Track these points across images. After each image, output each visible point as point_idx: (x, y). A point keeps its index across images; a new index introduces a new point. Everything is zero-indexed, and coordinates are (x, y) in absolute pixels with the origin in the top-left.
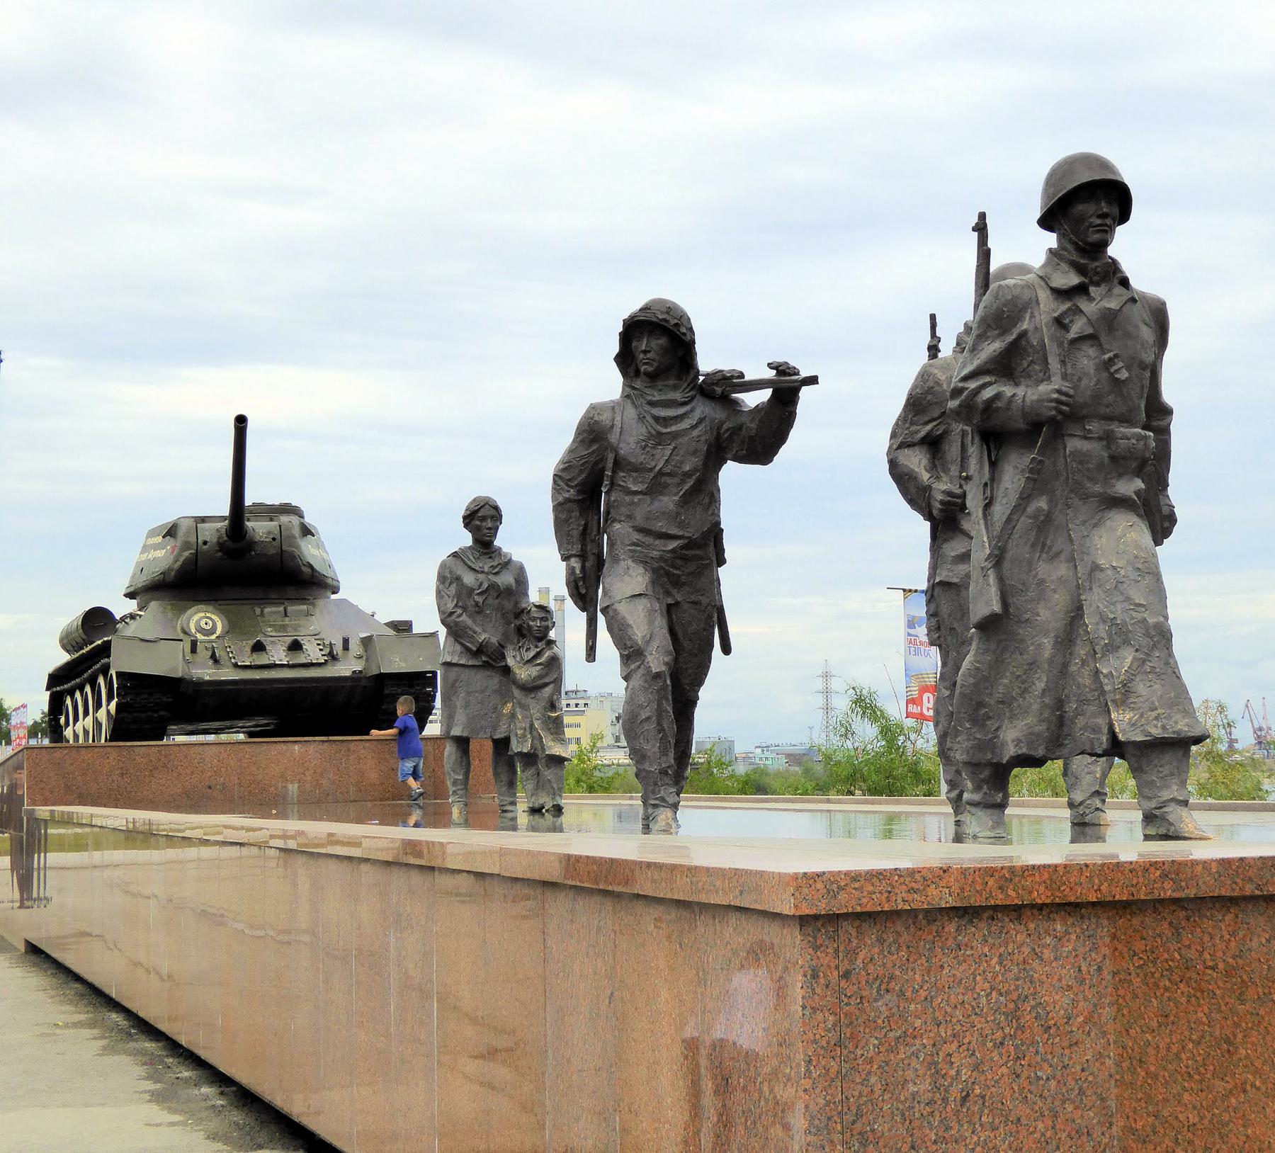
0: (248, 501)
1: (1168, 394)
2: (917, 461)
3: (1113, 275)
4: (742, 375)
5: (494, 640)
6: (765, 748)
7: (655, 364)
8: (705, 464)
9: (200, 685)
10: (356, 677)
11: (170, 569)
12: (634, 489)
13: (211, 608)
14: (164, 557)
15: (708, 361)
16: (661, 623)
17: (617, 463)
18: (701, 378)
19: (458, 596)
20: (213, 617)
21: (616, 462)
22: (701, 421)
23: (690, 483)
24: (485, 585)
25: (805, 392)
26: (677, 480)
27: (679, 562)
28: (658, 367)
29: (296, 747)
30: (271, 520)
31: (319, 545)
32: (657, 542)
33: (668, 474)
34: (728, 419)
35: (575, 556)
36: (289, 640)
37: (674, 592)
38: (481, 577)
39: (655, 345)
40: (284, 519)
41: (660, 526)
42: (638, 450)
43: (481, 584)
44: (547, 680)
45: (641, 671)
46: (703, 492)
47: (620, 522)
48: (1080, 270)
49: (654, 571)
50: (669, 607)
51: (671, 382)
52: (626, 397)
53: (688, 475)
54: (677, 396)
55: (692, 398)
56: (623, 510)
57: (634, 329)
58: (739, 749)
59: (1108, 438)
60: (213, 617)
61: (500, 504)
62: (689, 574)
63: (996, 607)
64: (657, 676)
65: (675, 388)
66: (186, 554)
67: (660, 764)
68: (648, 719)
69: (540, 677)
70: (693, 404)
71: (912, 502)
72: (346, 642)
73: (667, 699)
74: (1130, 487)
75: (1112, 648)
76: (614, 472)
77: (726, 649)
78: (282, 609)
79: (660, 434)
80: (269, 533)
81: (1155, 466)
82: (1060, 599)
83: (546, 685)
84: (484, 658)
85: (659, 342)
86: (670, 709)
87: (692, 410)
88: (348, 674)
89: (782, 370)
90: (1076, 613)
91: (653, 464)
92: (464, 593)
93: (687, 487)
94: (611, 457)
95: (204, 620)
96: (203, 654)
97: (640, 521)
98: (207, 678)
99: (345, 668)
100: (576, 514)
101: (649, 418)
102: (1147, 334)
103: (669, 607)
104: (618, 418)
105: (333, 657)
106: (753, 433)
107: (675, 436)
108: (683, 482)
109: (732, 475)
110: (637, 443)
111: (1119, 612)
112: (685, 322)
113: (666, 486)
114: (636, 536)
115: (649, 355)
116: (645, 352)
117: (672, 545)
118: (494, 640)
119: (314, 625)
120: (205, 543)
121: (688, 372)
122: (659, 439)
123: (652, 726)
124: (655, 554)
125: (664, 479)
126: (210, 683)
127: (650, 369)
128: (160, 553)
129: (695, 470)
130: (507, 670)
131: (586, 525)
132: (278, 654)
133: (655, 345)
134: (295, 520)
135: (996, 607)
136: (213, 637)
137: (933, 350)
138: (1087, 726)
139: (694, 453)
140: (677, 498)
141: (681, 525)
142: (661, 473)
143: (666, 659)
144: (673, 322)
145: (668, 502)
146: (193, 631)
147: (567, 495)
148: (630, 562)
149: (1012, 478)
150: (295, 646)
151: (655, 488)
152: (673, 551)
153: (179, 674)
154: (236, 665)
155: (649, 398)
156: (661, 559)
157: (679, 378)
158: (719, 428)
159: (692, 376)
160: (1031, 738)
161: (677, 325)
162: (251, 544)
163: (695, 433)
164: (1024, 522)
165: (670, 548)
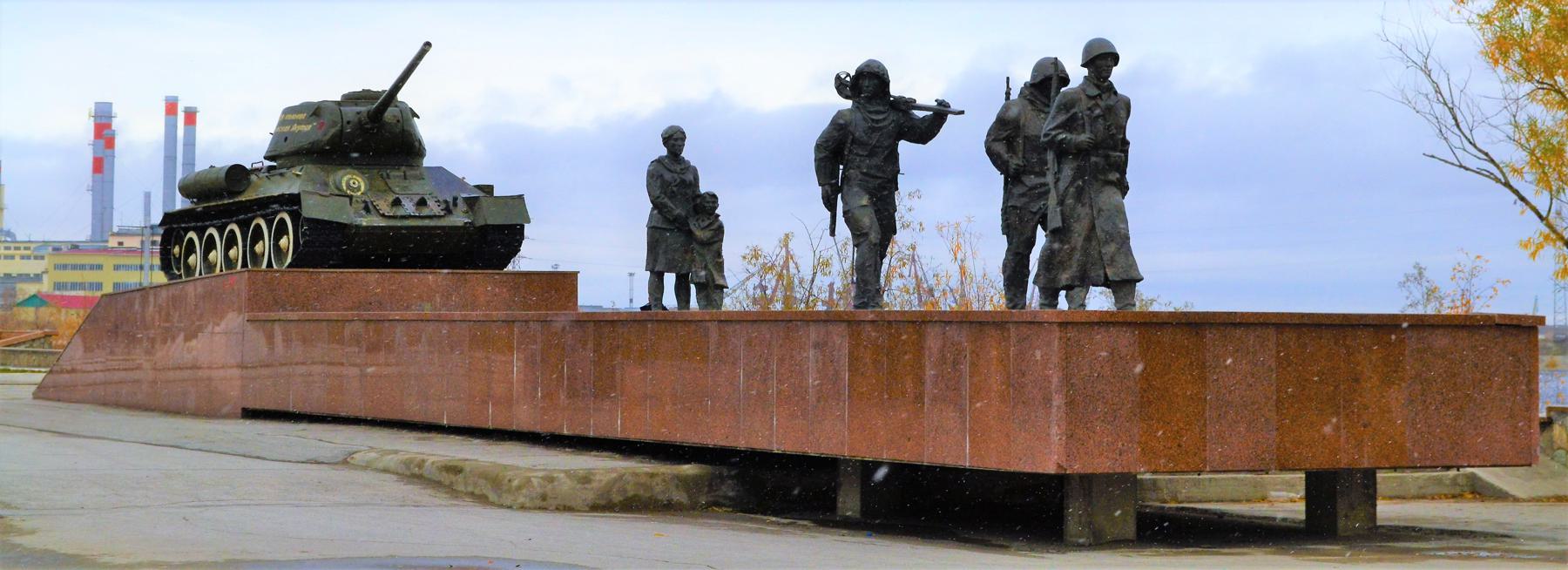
0: (401, 96)
1: (1128, 137)
2: (1000, 148)
3: (1111, 89)
10: (465, 227)
15: (895, 90)
17: (853, 141)
19: (662, 187)
39: (867, 85)
48: (1098, 87)
59: (1107, 157)
63: (1060, 224)
66: (333, 131)
71: (995, 163)
72: (455, 199)
74: (1114, 176)
75: (1107, 242)
81: (1122, 167)
82: (1085, 223)
90: (1093, 228)
95: (353, 180)
99: (459, 219)
102: (1123, 114)
105: (448, 211)
107: (880, 129)
109: (906, 150)
111: (1108, 228)
122: (873, 130)
128: (306, 128)
130: (690, 233)
135: (1060, 224)
137: (1008, 94)
138: (1096, 273)
145: (876, 161)
149: (1068, 171)
150: (422, 203)
160: (1073, 278)
164: (1072, 190)
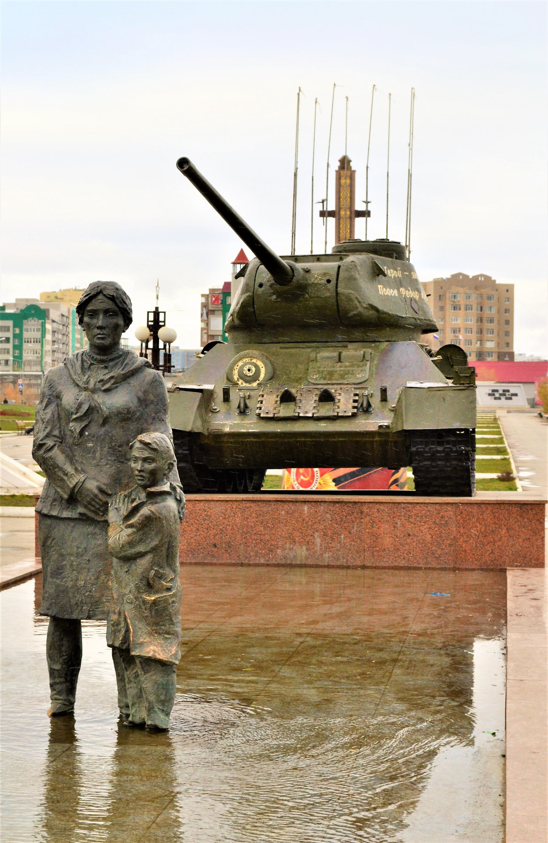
5: (92, 485)
9: (218, 436)
10: (383, 432)
13: (256, 352)
20: (260, 364)
24: (85, 407)
29: (306, 508)
38: (84, 395)
43: (80, 406)
44: (141, 548)
60: (260, 364)
61: (54, 291)
66: (245, 296)
69: (131, 544)
78: (336, 354)
80: (325, 274)
83: (141, 555)
84: (81, 510)
88: (374, 428)
92: (62, 417)
98: (227, 430)
105: (365, 409)
118: (92, 485)
120: (261, 285)
136: (255, 384)
146: (236, 377)
150: (326, 397)
153: (188, 429)
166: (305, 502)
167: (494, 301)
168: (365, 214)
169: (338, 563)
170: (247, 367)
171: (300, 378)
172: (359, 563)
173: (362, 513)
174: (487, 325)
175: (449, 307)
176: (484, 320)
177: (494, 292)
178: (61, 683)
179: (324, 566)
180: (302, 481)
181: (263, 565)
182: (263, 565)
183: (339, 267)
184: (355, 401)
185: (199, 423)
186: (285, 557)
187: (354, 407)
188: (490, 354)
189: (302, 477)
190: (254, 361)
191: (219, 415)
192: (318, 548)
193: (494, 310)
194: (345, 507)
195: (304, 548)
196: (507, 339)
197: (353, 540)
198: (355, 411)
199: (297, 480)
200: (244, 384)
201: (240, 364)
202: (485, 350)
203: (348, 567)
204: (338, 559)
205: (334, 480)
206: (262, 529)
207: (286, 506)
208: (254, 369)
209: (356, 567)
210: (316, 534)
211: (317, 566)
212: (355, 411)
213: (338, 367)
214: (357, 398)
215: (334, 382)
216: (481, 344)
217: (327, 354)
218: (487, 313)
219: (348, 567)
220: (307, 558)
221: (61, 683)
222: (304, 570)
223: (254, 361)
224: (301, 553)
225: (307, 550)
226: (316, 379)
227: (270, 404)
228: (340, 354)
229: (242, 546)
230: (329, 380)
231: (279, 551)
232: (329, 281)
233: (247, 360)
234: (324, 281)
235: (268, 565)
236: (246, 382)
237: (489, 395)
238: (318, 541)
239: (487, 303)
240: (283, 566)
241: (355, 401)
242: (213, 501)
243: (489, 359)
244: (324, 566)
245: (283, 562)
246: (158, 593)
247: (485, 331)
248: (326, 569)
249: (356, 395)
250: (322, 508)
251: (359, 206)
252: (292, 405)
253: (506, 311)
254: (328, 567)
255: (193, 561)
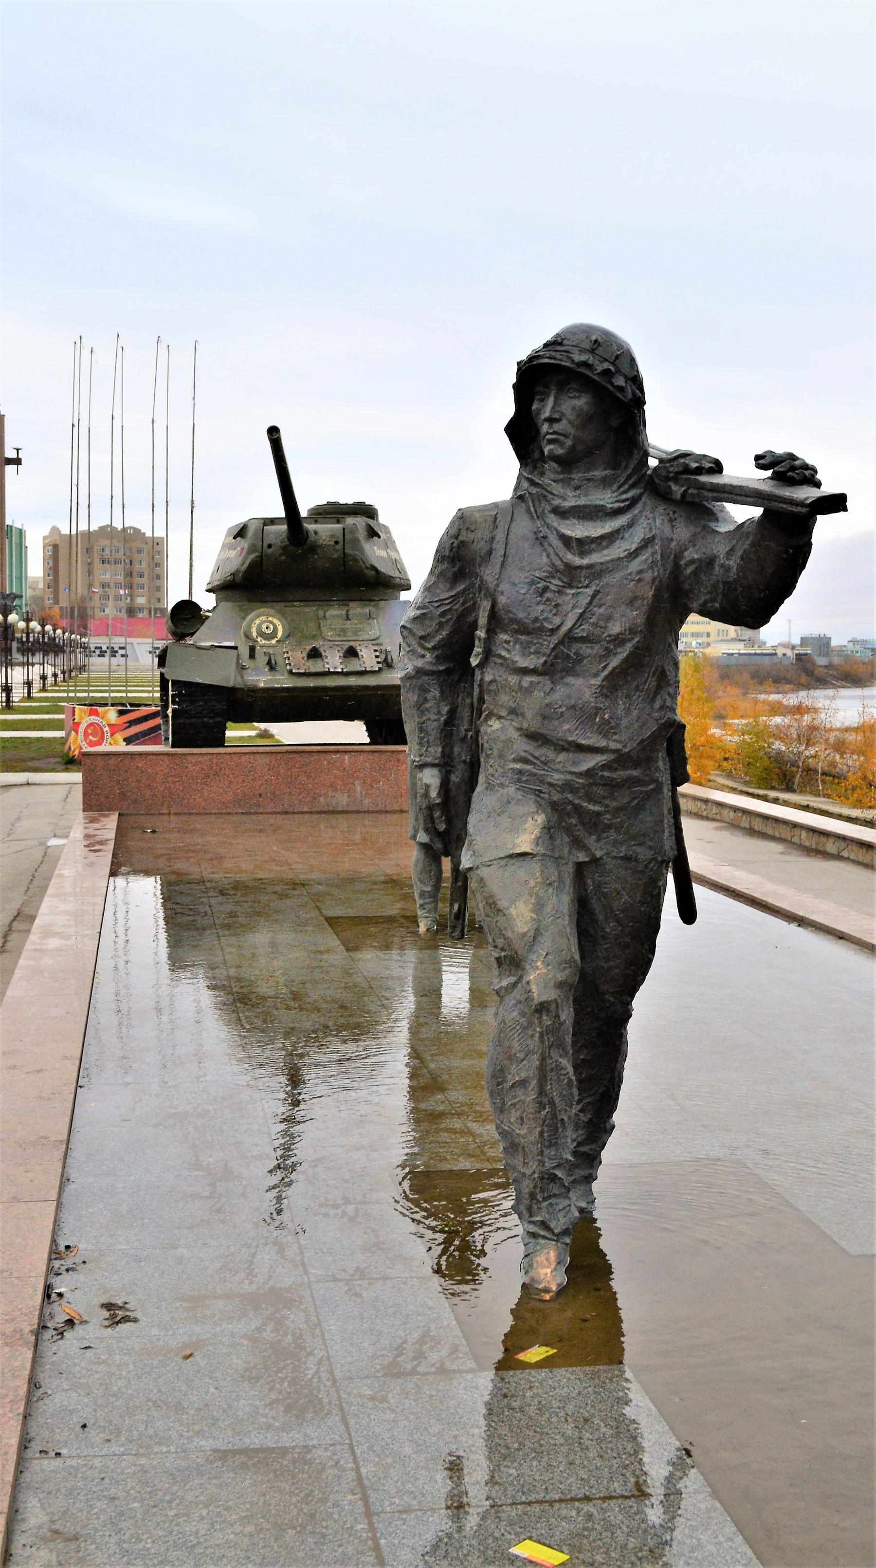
4: (717, 467)
6: (854, 642)
7: (569, 442)
8: (650, 622)
9: (253, 691)
11: (238, 571)
12: (523, 663)
14: (237, 559)
15: (667, 429)
16: (562, 903)
18: (653, 462)
20: (276, 621)
21: (493, 615)
22: (646, 543)
23: (623, 653)
25: (825, 527)
26: (597, 649)
27: (600, 791)
28: (573, 448)
29: (346, 757)
30: (338, 522)
31: (389, 544)
32: (562, 757)
33: (583, 640)
34: (693, 541)
35: (433, 765)
36: (346, 645)
37: (591, 841)
39: (576, 402)
40: (350, 521)
41: (568, 730)
42: (532, 597)
45: (517, 994)
46: (649, 661)
47: (500, 718)
49: (554, 806)
50: (580, 867)
51: (598, 473)
52: (519, 497)
53: (619, 640)
54: (606, 498)
55: (634, 502)
56: (504, 698)
57: (535, 378)
58: (834, 643)
60: (276, 621)
62: (617, 810)
64: (542, 1008)
65: (605, 483)
66: (252, 556)
67: (542, 1163)
68: (523, 1083)
70: (636, 511)
73: (561, 1046)
76: (491, 631)
77: (688, 913)
78: (344, 612)
79: (570, 569)
80: (332, 536)
85: (575, 404)
86: (567, 1064)
87: (630, 525)
89: (789, 470)
91: (557, 620)
93: (614, 662)
94: (485, 606)
95: (267, 622)
96: (261, 660)
97: (531, 722)
98: (262, 685)
100: (435, 692)
101: (553, 539)
103: (580, 867)
104: (500, 536)
105: (388, 664)
106: (732, 575)
107: (596, 572)
108: (609, 653)
110: (532, 583)
112: (625, 368)
113: (580, 658)
114: (523, 746)
115: (557, 427)
116: (551, 420)
117: (590, 762)
119: (374, 629)
120: (270, 546)
121: (631, 453)
122: (571, 576)
123: (529, 1096)
124: (557, 777)
125: (576, 646)
126: (266, 690)
127: (559, 451)
129: (632, 631)
131: (452, 713)
132: (334, 661)
133: (576, 402)
134: (360, 522)
136: (274, 641)
139: (631, 602)
140: (597, 681)
141: (607, 729)
142: (570, 638)
143: (561, 977)
144: (600, 367)
145: (583, 687)
146: (254, 635)
147: (420, 663)
148: (511, 790)
150: (352, 653)
151: (556, 667)
152: (589, 773)
153: (231, 684)
154: (290, 672)
155: (557, 502)
156: (567, 786)
157: (615, 466)
158: (678, 556)
159: (637, 456)
161: (607, 372)
162: (314, 548)
163: (635, 565)
165: (584, 767)
166: (346, 752)
167: (144, 555)
168: (17, 461)
169: (378, 809)
170: (264, 626)
171: (315, 636)
172: (397, 808)
173: (399, 761)
174: (137, 580)
175: (97, 561)
176: (134, 574)
177: (144, 546)
178: (430, 903)
179: (365, 812)
180: (91, 741)
181: (307, 813)
182: (307, 813)
183: (344, 529)
184: (377, 657)
185: (239, 679)
186: (328, 805)
187: (378, 663)
188: (141, 610)
189: (91, 737)
190: (270, 619)
191: (249, 671)
192: (358, 795)
193: (144, 564)
194: (383, 756)
195: (346, 795)
196: (158, 595)
197: (390, 787)
198: (380, 665)
199: (85, 740)
200: (264, 642)
201: (257, 622)
202: (135, 606)
203: (387, 812)
204: (377, 805)
205: (125, 740)
206: (305, 778)
207: (328, 756)
208: (272, 627)
209: (393, 812)
210: (357, 782)
211: (358, 812)
212: (380, 665)
213: (348, 624)
214: (378, 654)
215: (349, 638)
216: (131, 600)
217: (335, 612)
218: (137, 567)
219: (387, 812)
220: (348, 805)
221: (430, 903)
222: (345, 816)
223: (270, 619)
224: (342, 800)
225: (348, 797)
226: (331, 636)
227: (298, 659)
228: (347, 611)
229: (286, 796)
230: (345, 636)
231: (322, 799)
232: (337, 543)
233: (263, 618)
234: (332, 543)
235: (311, 813)
236: (265, 639)
237: (150, 652)
238: (359, 788)
239: (137, 557)
240: (325, 812)
241: (377, 657)
242: (258, 753)
243: (140, 615)
244: (365, 812)
245: (326, 809)
246: (842, 803)
247: (135, 586)
248: (366, 815)
249: (375, 651)
250: (362, 757)
251: (10, 454)
252: (319, 661)
253: (157, 565)
254: (368, 812)
255: (240, 811)
